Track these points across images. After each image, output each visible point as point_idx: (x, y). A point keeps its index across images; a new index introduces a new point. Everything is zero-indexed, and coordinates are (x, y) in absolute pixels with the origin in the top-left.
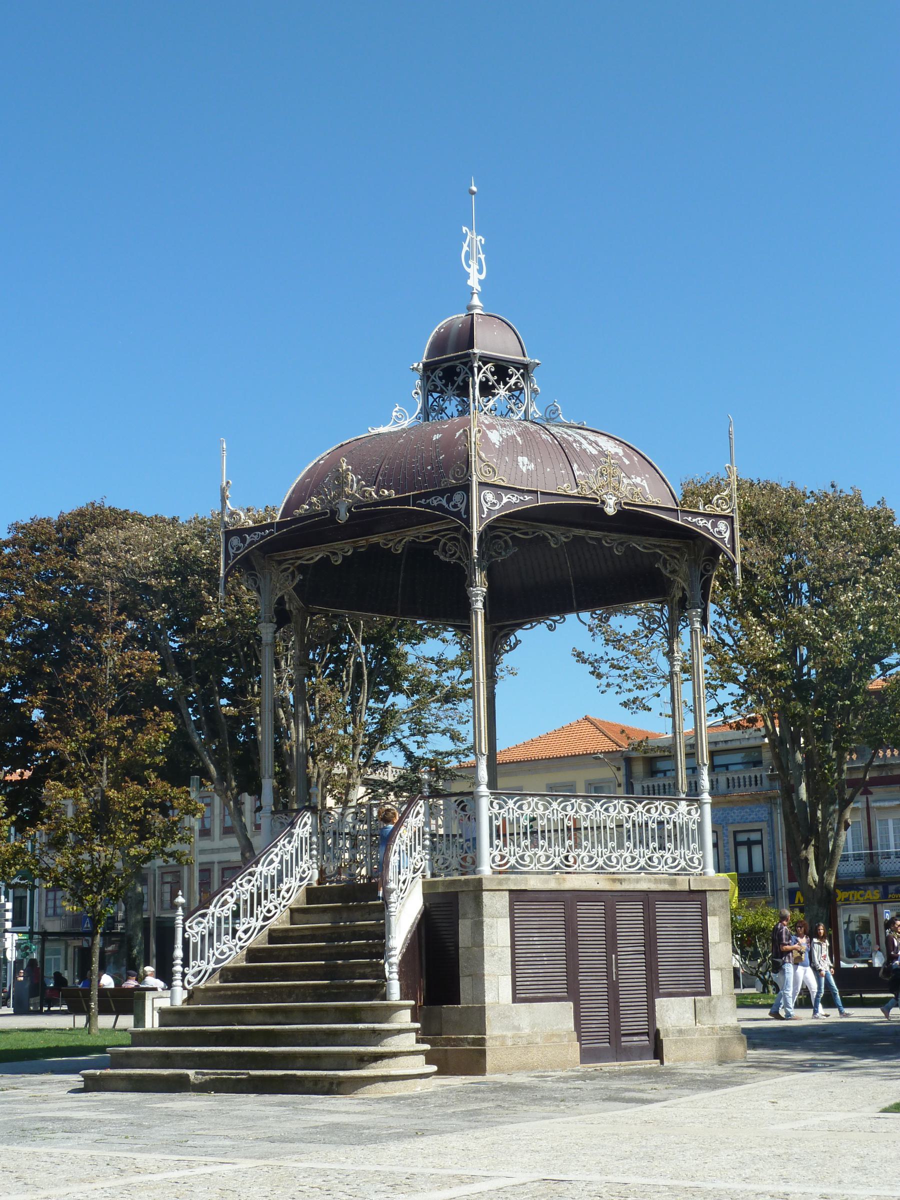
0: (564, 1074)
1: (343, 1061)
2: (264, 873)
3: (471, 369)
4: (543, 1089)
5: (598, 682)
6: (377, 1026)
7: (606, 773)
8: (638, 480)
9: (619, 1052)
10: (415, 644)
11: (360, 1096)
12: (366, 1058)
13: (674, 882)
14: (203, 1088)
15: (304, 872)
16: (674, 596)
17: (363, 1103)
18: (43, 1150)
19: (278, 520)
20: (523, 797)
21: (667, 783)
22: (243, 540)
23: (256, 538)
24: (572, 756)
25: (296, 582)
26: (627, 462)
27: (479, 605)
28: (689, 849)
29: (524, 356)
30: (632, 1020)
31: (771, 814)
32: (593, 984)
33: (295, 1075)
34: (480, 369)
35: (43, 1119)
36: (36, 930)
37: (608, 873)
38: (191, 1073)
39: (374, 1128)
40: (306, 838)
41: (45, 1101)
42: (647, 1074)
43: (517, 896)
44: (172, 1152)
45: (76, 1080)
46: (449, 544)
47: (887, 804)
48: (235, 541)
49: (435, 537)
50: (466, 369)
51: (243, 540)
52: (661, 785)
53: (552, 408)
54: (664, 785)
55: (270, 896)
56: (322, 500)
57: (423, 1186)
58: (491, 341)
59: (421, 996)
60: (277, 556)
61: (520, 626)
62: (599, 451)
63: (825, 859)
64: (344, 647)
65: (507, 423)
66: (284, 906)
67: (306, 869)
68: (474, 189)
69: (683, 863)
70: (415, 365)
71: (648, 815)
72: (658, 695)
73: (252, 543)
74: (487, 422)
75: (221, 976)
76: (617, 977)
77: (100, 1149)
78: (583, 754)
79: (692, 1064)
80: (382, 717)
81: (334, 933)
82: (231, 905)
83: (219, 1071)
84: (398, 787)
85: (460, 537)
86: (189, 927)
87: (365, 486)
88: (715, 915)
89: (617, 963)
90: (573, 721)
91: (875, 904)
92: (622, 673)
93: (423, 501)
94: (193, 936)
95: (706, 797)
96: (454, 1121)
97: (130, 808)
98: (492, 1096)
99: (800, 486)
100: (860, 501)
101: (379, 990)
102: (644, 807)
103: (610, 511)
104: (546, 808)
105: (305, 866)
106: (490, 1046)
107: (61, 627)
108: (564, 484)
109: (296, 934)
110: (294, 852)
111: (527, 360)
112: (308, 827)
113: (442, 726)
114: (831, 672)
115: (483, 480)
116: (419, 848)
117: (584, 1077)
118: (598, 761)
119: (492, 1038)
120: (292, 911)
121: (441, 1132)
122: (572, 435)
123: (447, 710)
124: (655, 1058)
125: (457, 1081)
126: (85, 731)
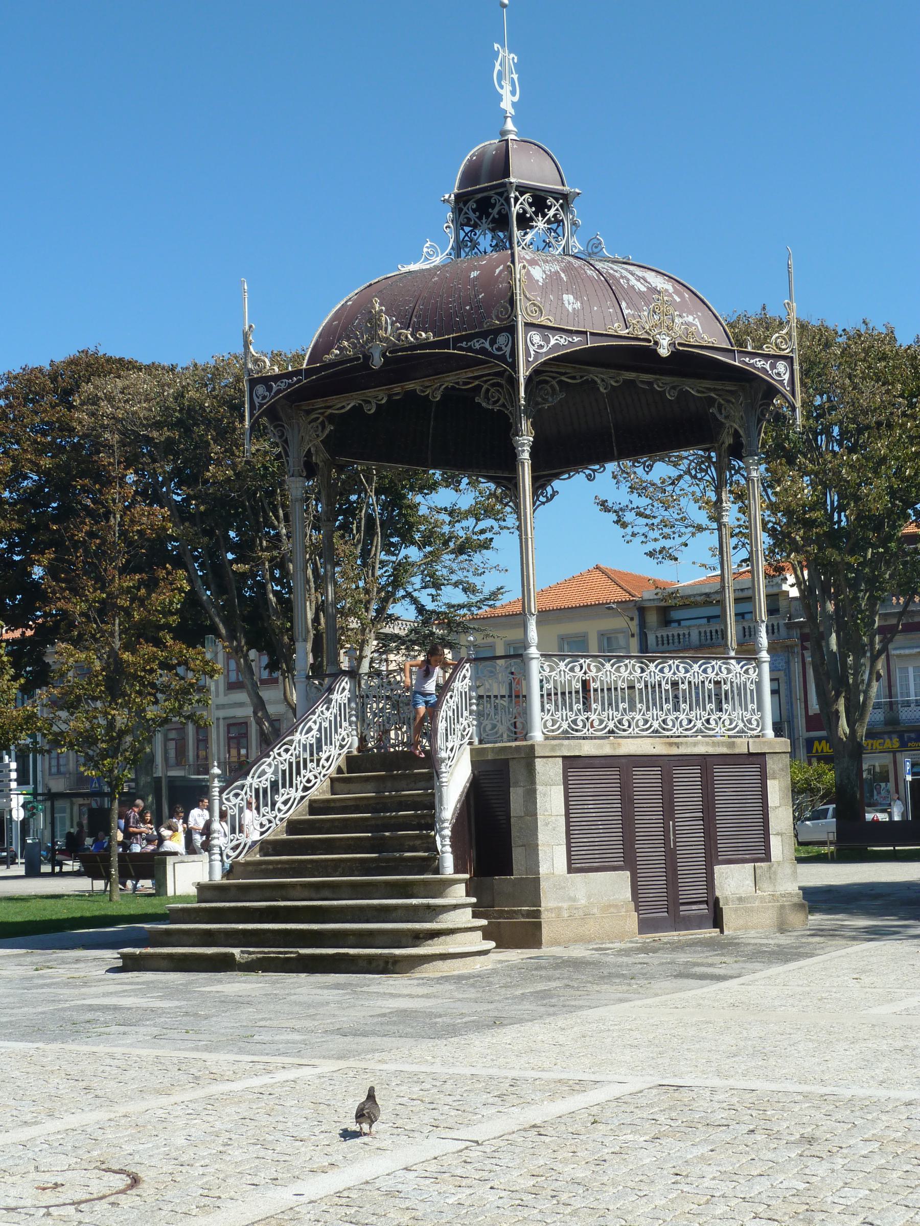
0: (622, 946)
1: (397, 938)
2: (303, 741)
3: (507, 200)
4: (606, 965)
5: (622, 531)
6: (432, 901)
7: (619, 623)
8: (690, 319)
9: (679, 922)
10: (426, 494)
11: (418, 975)
12: (421, 936)
13: (733, 745)
14: (249, 967)
15: (343, 739)
16: (723, 443)
17: (424, 984)
18: (101, 1049)
19: (304, 366)
20: (575, 659)
21: (681, 633)
22: (269, 389)
23: (283, 386)
24: (584, 606)
25: (327, 432)
26: (678, 300)
29: (563, 185)
30: (690, 888)
31: (788, 663)
32: (650, 852)
33: (347, 954)
34: (516, 199)
35: (91, 1008)
36: (40, 791)
37: (665, 737)
38: (236, 951)
39: (445, 1015)
40: (345, 704)
41: (85, 984)
42: (710, 944)
43: (571, 762)
44: (241, 1051)
45: (111, 956)
46: (492, 390)
47: (907, 652)
48: (260, 389)
49: (477, 383)
50: (502, 201)
51: (269, 389)
52: (676, 634)
53: (595, 241)
54: (679, 635)
55: (309, 765)
56: (353, 343)
57: (533, 1097)
58: (528, 170)
59: (471, 866)
60: (305, 405)
61: (557, 476)
62: (648, 288)
63: (855, 711)
64: (353, 498)
65: (549, 258)
66: (324, 776)
67: (346, 737)
69: (741, 725)
70: (447, 196)
71: (704, 675)
72: (686, 545)
73: (279, 391)
74: (528, 258)
75: (261, 850)
76: (674, 844)
77: (163, 1047)
78: (595, 604)
79: (753, 933)
80: (395, 569)
81: (378, 803)
82: (269, 775)
83: (266, 950)
84: (409, 641)
85: (503, 382)
86: (226, 799)
87: (401, 328)
88: (774, 778)
89: (674, 830)
90: (584, 570)
91: (894, 752)
92: (650, 521)
93: (464, 344)
94: (231, 808)
95: (764, 655)
96: (526, 1005)
97: (144, 670)
98: (557, 973)
99: (831, 324)
100: (891, 337)
101: (431, 864)
102: (700, 667)
103: (664, 352)
104: (599, 670)
105: (344, 733)
106: (546, 918)
107: (59, 483)
108: (613, 324)
109: (338, 804)
110: (332, 719)
111: (567, 189)
112: (346, 692)
113: (454, 578)
114: (866, 520)
115: (529, 320)
116: (466, 714)
117: (645, 949)
118: (611, 611)
119: (547, 910)
120: (332, 780)
121: (521, 1021)
122: (619, 271)
123: (462, 562)
124: (714, 927)
125: (514, 956)
126: (95, 591)
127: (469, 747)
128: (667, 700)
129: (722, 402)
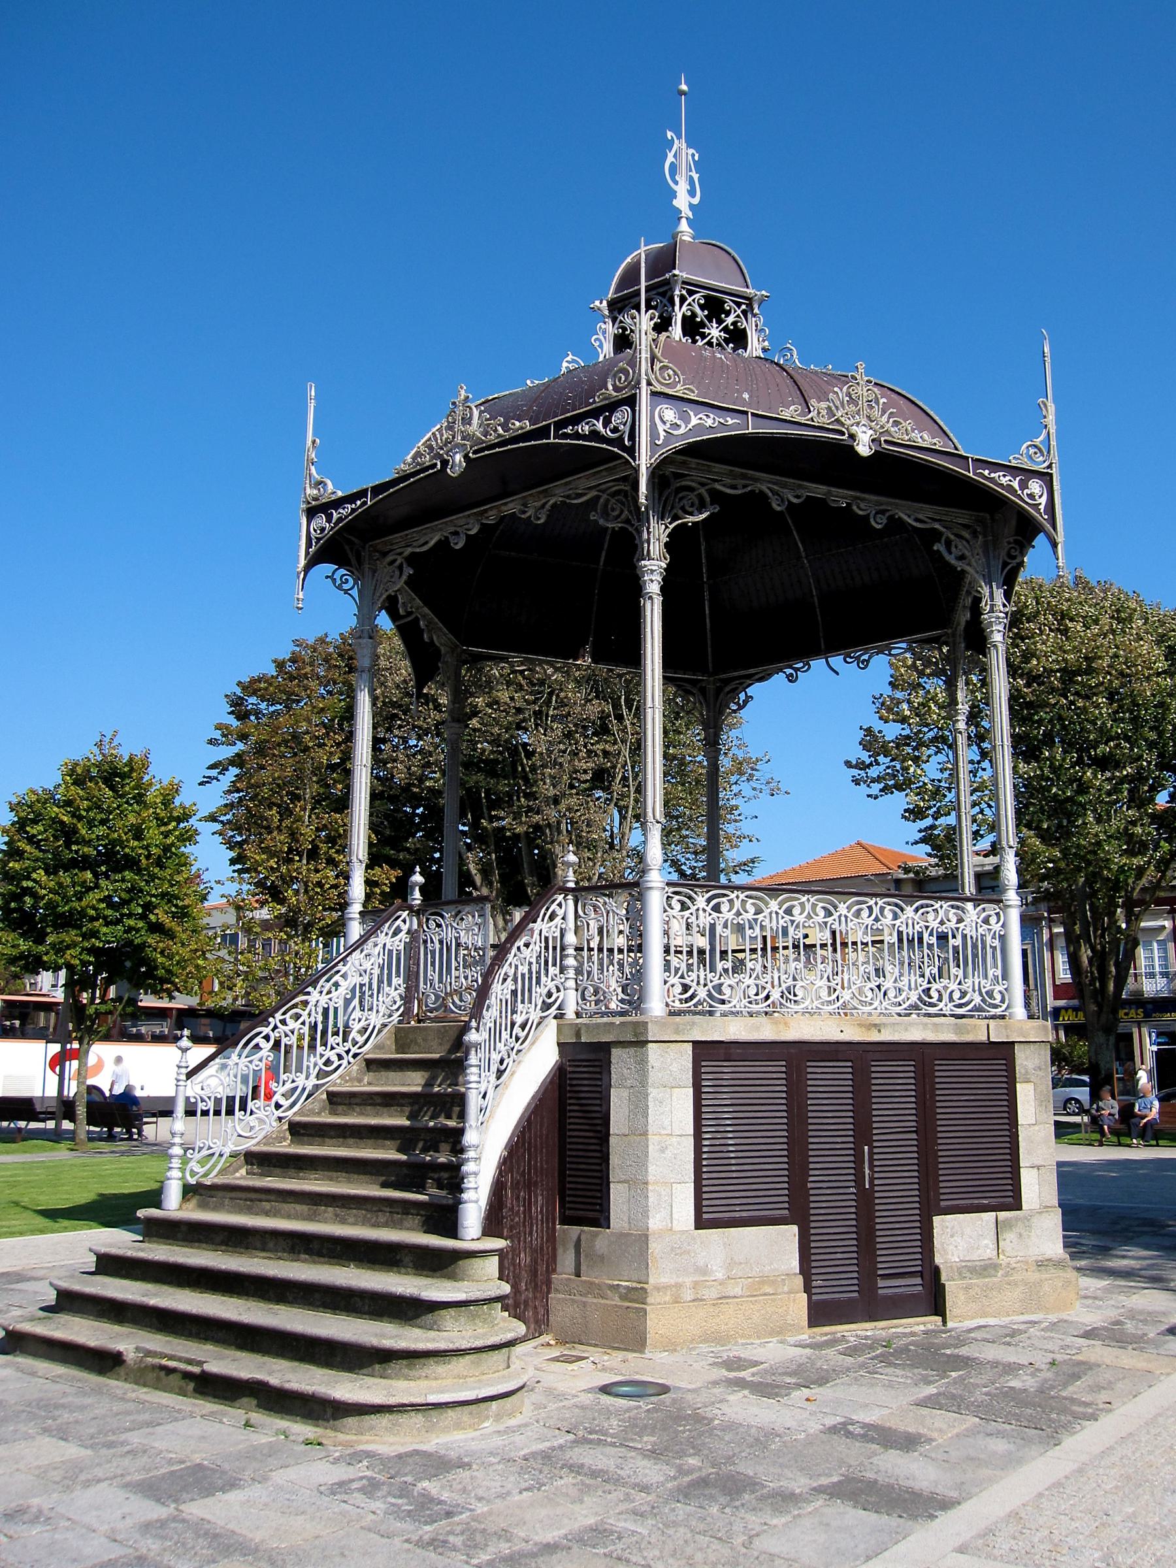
9: (870, 1306)
22: (329, 518)
27: (653, 587)
28: (986, 977)
34: (683, 299)
43: (704, 1051)
50: (665, 301)
68: (684, 87)
73: (340, 520)
89: (871, 1160)
90: (846, 846)
93: (569, 430)
95: (1012, 897)
102: (917, 910)
111: (750, 291)
119: (658, 1289)
127: (555, 1022)
129: (952, 537)
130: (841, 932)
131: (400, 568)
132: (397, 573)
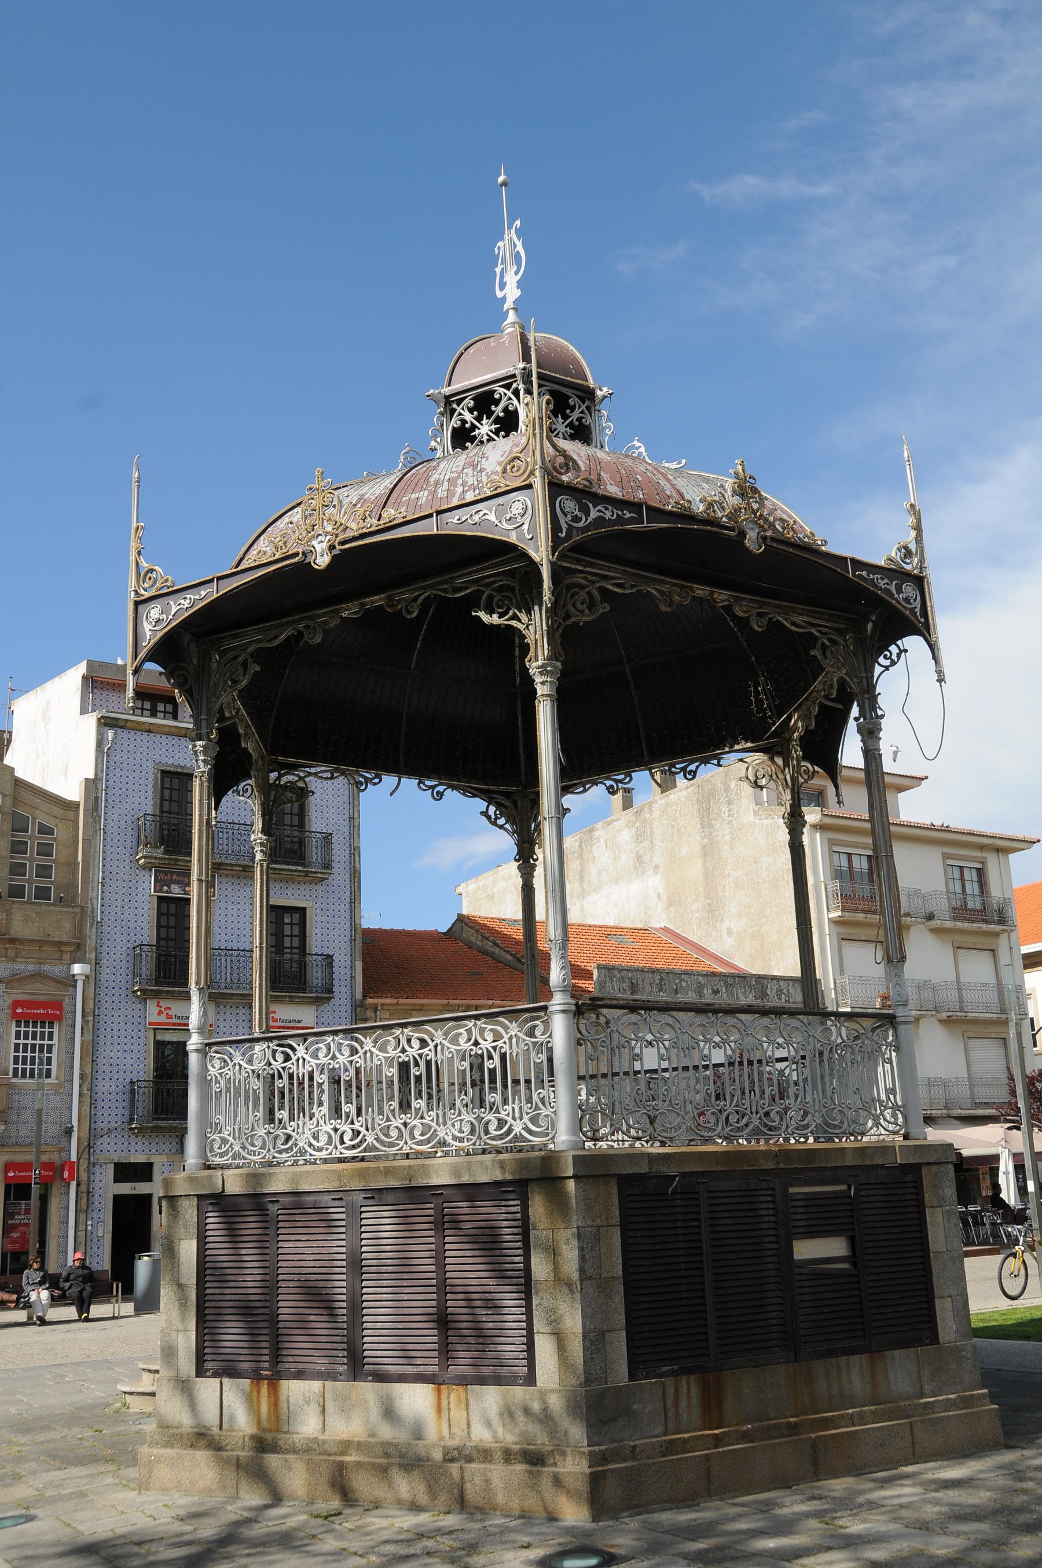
50: (509, 394)
128: (349, 1083)
130: (436, 1062)
131: (245, 664)
132: (241, 669)
